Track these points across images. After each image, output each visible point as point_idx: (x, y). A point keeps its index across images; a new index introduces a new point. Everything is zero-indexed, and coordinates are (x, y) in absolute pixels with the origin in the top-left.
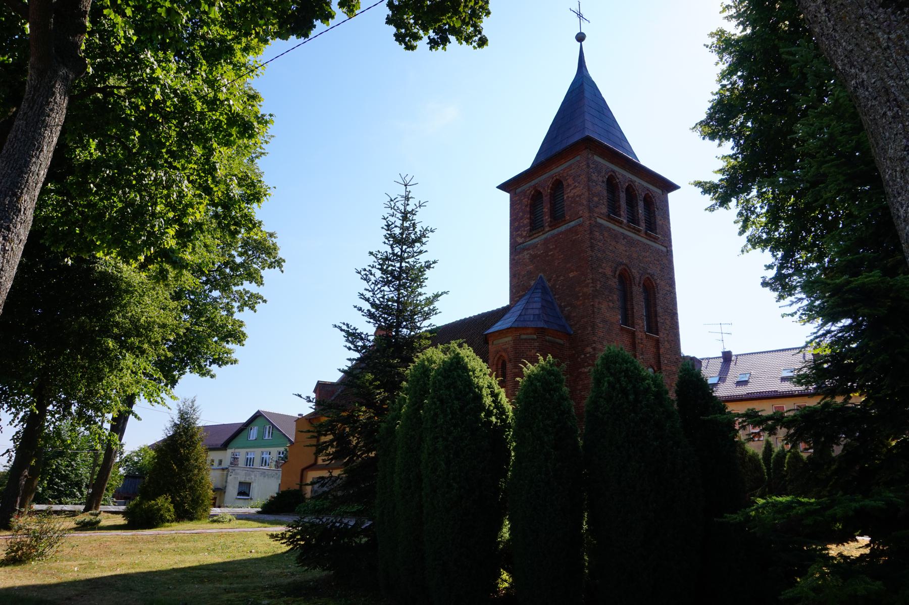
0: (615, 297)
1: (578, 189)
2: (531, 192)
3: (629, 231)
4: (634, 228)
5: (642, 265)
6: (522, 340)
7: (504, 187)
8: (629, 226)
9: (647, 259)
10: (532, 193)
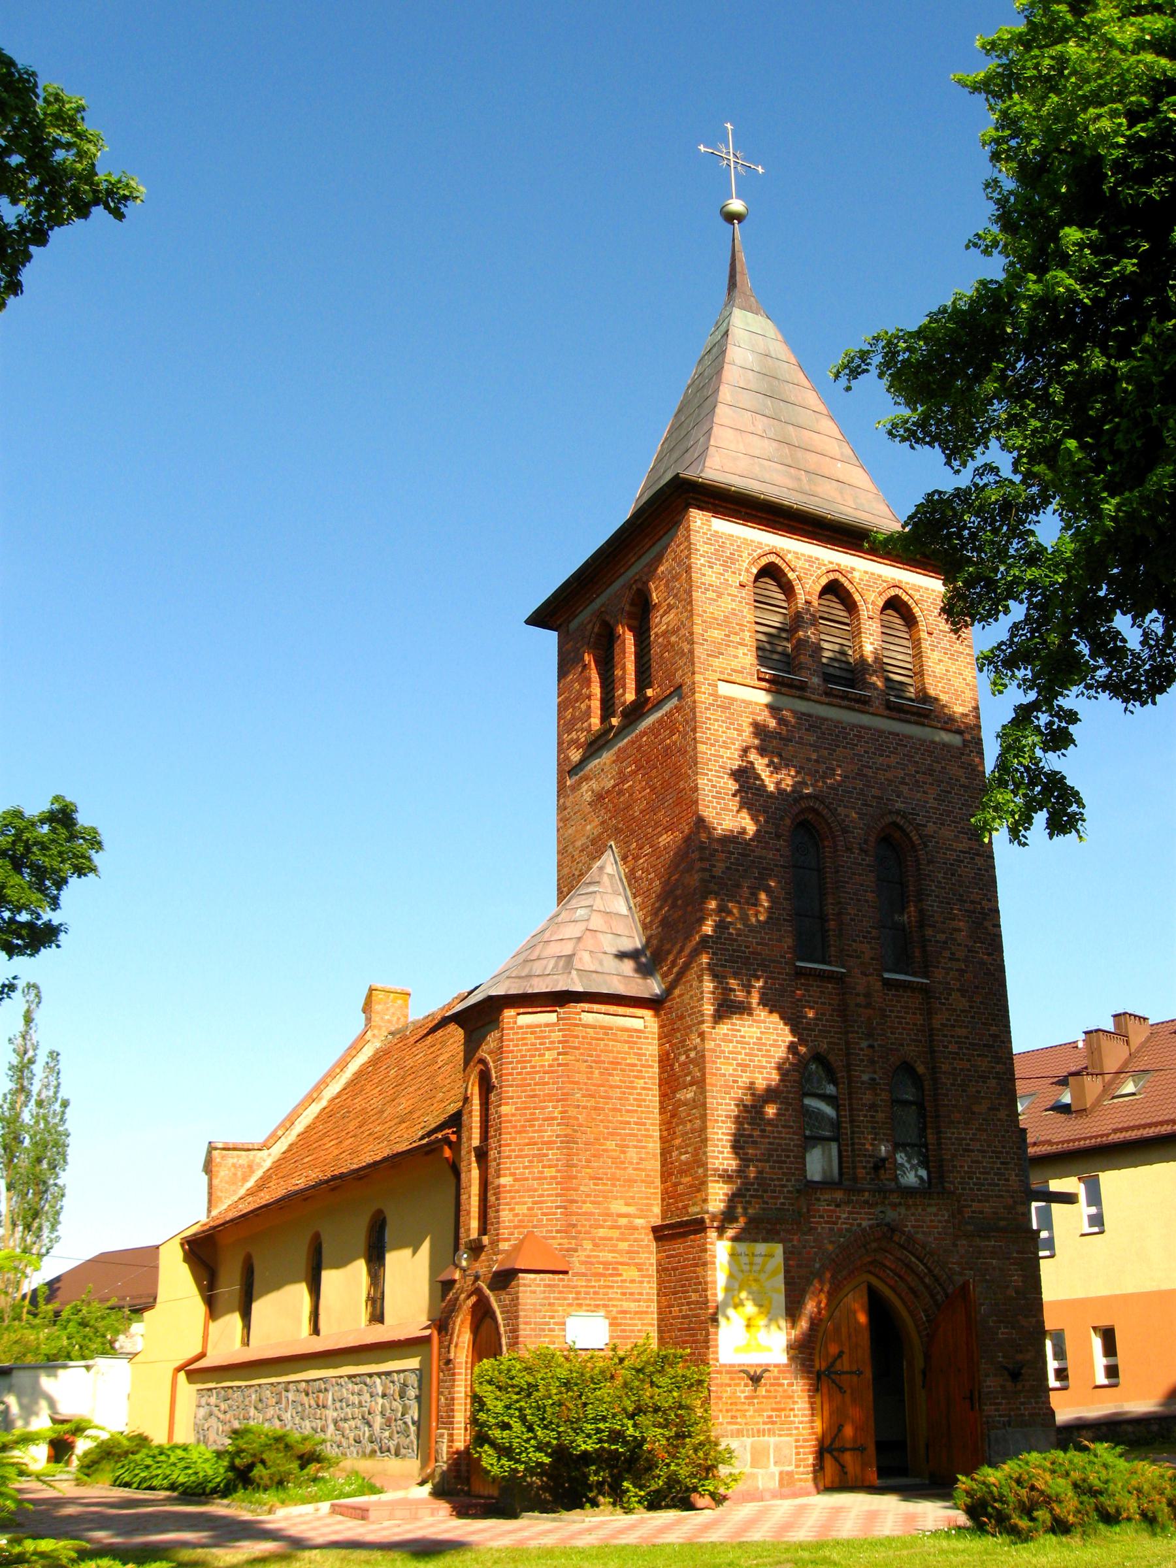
3: (830, 704)
4: (844, 696)
5: (874, 792)
6: (521, 1027)
7: (540, 619)
8: (828, 693)
9: (889, 775)
10: (596, 630)
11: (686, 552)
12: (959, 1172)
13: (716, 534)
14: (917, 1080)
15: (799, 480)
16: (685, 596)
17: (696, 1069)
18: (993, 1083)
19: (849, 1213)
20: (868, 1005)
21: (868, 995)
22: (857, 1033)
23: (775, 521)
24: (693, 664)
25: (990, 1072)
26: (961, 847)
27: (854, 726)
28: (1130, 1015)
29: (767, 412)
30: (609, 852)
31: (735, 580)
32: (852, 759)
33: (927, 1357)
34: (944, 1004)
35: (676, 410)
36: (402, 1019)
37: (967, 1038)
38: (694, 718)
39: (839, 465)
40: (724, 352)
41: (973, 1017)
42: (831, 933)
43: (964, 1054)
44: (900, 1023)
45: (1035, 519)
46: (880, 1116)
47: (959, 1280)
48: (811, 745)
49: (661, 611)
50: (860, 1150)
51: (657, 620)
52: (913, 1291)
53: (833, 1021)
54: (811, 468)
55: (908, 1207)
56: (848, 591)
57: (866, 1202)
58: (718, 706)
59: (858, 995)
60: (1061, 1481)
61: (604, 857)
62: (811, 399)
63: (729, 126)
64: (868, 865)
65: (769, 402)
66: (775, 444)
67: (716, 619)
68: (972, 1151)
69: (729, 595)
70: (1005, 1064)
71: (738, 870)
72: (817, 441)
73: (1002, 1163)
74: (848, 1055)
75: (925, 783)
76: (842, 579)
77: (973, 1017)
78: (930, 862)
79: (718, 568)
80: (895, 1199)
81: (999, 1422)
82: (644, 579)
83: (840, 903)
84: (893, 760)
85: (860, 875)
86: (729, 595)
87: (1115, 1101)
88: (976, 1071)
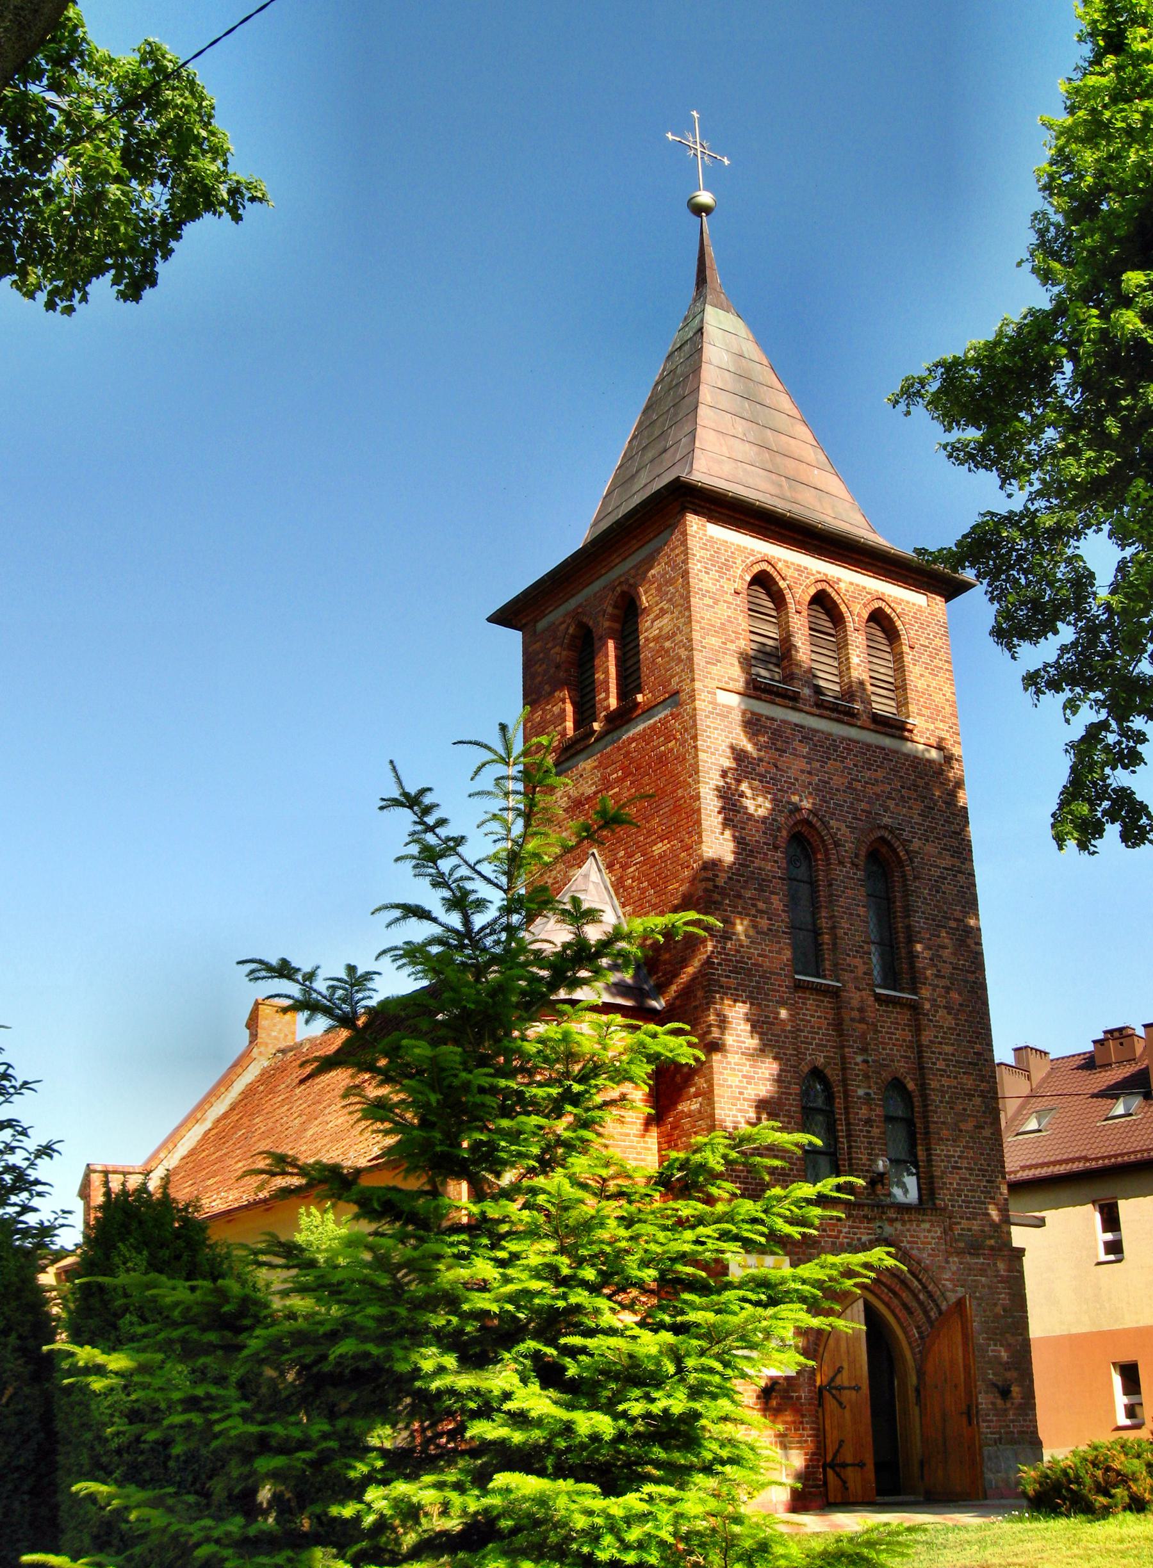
0: (777, 902)
1: (668, 617)
2: (567, 628)
3: (821, 716)
5: (863, 805)
7: (505, 617)
10: (571, 631)
11: (682, 557)
12: (948, 1189)
13: (711, 540)
14: (907, 1096)
15: (781, 486)
16: (682, 602)
17: (702, 1080)
18: (978, 1100)
19: (850, 1227)
20: (862, 1020)
21: (861, 1010)
22: (852, 1047)
23: (766, 529)
24: (692, 671)
25: (975, 1090)
26: (944, 864)
27: (844, 739)
28: (1032, 1049)
29: (745, 415)
30: (591, 859)
31: (730, 587)
32: (843, 772)
33: (921, 1373)
34: (931, 1021)
35: (643, 406)
36: (290, 1036)
37: (953, 1055)
38: (695, 725)
39: (816, 471)
40: (700, 351)
41: (958, 1035)
42: (825, 947)
43: (951, 1072)
44: (890, 1039)
45: (1076, 544)
46: (876, 1131)
47: (953, 1298)
48: (804, 757)
49: (652, 616)
50: (857, 1164)
51: (649, 623)
52: (905, 1306)
53: (828, 1035)
54: (791, 474)
55: (904, 1223)
56: (834, 602)
57: (865, 1217)
58: (718, 714)
59: (852, 1009)
60: (1136, 1461)
61: (585, 866)
62: (785, 402)
63: (694, 113)
64: (859, 880)
65: (746, 404)
66: (755, 448)
67: (713, 626)
68: (960, 1168)
69: (725, 601)
70: (988, 1082)
71: (739, 881)
72: (794, 446)
73: (988, 1181)
74: (844, 1069)
75: (910, 798)
76: (830, 590)
77: (958, 1035)
78: (916, 878)
79: (714, 574)
80: (892, 1214)
81: (991, 1439)
82: (632, 581)
83: (834, 916)
84: (880, 774)
85: (852, 889)
86: (725, 601)
87: (1020, 1137)
88: (962, 1089)
